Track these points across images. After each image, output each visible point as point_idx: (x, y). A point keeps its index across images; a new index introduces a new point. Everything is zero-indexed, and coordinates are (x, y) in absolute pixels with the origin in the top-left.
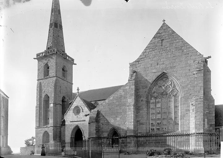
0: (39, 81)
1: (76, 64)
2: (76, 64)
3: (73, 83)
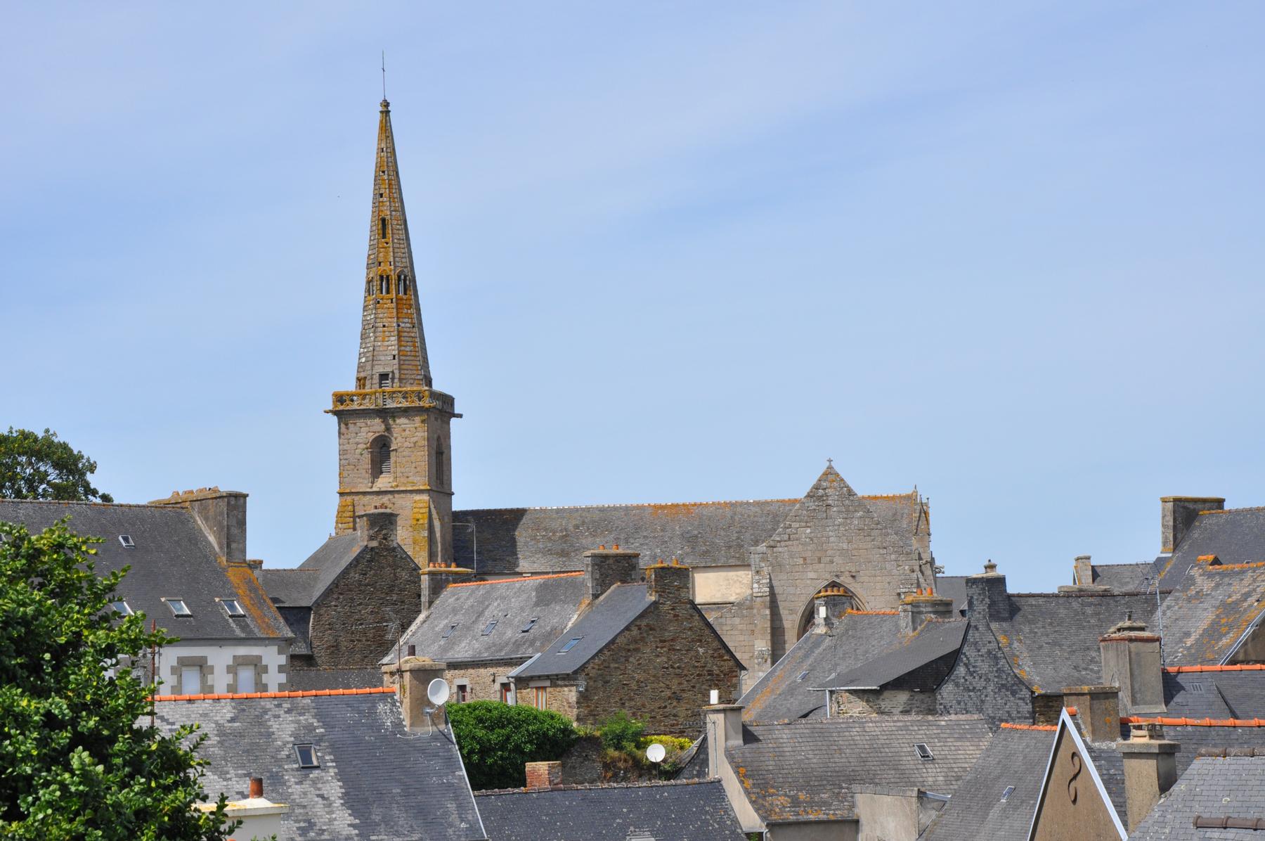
0: (349, 499)
1: (460, 416)
2: (460, 416)
3: (452, 491)
